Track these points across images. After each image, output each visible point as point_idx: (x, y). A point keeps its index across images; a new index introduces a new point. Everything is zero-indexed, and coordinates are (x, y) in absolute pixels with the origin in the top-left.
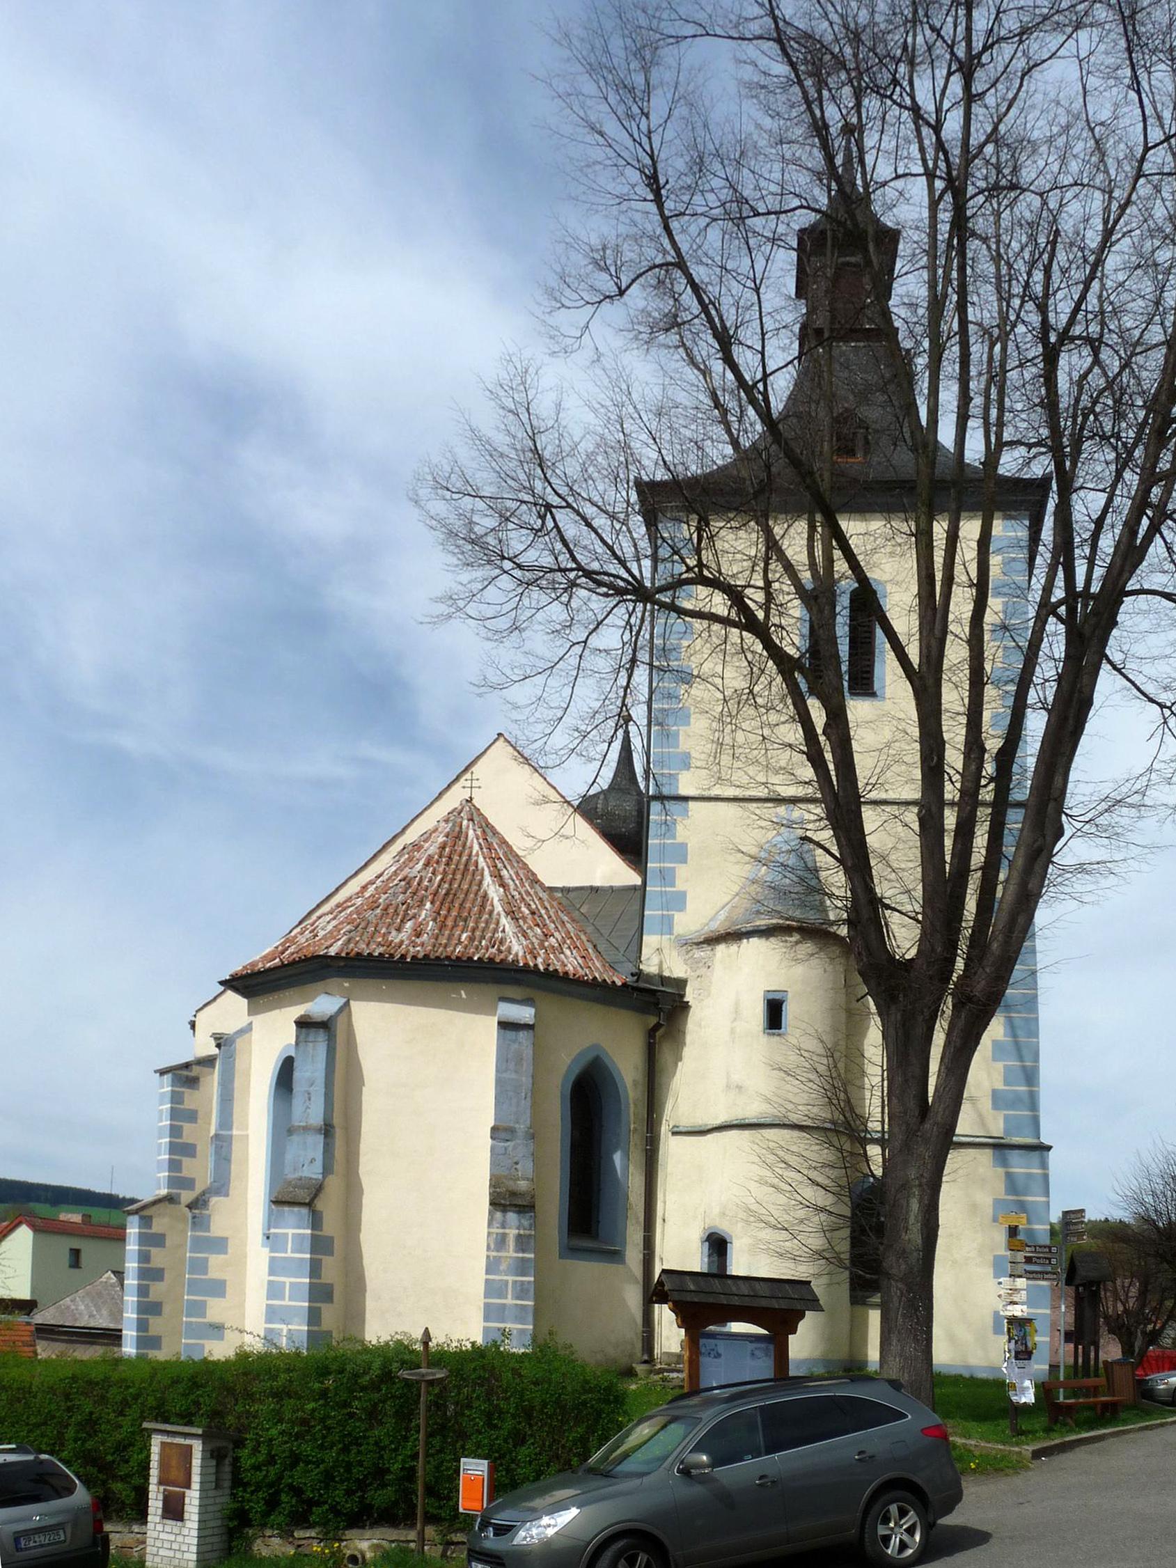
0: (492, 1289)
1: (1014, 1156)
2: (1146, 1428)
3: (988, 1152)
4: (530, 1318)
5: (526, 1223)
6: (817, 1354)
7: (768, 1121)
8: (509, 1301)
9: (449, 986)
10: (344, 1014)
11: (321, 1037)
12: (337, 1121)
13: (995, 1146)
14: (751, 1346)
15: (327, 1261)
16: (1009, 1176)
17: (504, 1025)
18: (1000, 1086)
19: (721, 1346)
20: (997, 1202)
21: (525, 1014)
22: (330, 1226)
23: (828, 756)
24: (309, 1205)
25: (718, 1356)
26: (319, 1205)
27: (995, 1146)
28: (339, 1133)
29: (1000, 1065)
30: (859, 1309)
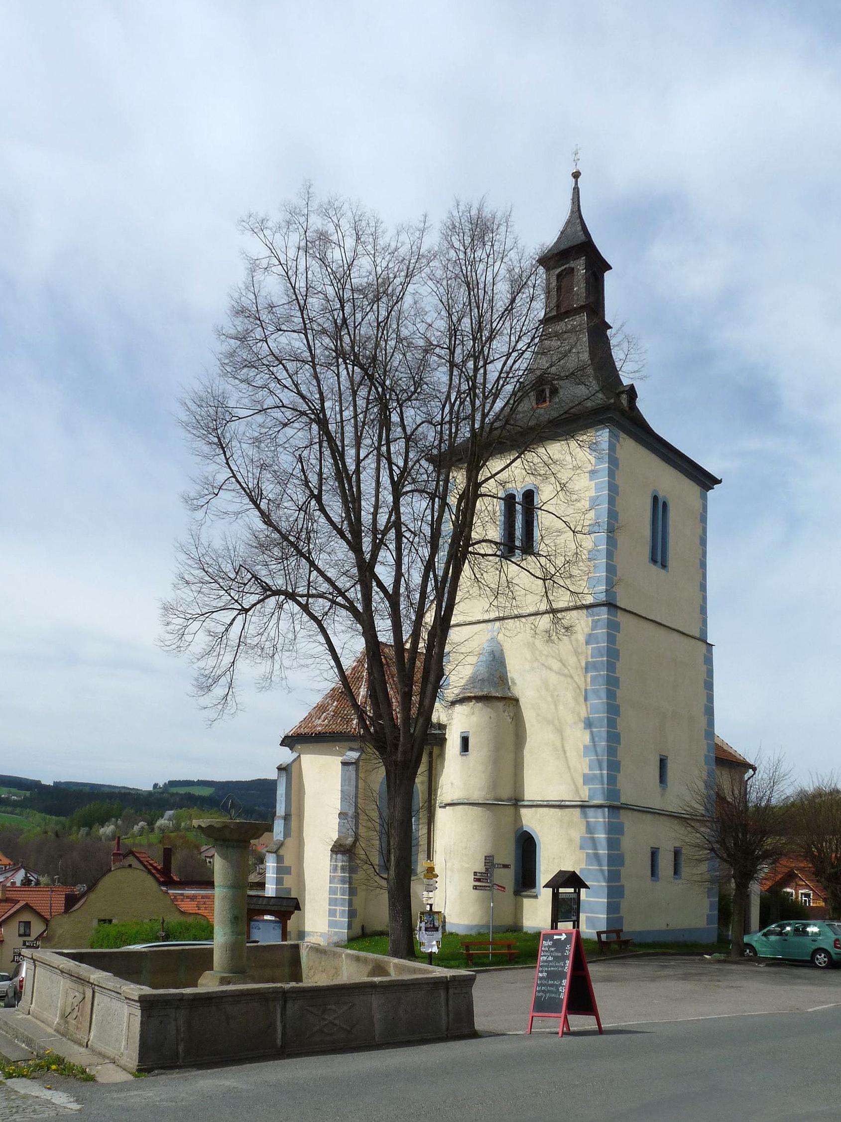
0: (332, 891)
1: (590, 812)
2: (528, 968)
3: (578, 810)
4: (347, 904)
5: (345, 859)
6: (483, 922)
7: (459, 801)
8: (339, 896)
9: (332, 744)
10: (298, 761)
11: (284, 774)
12: (294, 811)
13: (582, 807)
14: (273, 925)
15: (286, 877)
16: (587, 822)
17: (344, 764)
18: (587, 771)
19: (261, 925)
20: (581, 838)
21: (353, 755)
22: (287, 862)
23: (444, 605)
24: (275, 852)
25: (259, 929)
26: (281, 852)
27: (582, 807)
28: (294, 819)
29: (587, 759)
30: (519, 898)
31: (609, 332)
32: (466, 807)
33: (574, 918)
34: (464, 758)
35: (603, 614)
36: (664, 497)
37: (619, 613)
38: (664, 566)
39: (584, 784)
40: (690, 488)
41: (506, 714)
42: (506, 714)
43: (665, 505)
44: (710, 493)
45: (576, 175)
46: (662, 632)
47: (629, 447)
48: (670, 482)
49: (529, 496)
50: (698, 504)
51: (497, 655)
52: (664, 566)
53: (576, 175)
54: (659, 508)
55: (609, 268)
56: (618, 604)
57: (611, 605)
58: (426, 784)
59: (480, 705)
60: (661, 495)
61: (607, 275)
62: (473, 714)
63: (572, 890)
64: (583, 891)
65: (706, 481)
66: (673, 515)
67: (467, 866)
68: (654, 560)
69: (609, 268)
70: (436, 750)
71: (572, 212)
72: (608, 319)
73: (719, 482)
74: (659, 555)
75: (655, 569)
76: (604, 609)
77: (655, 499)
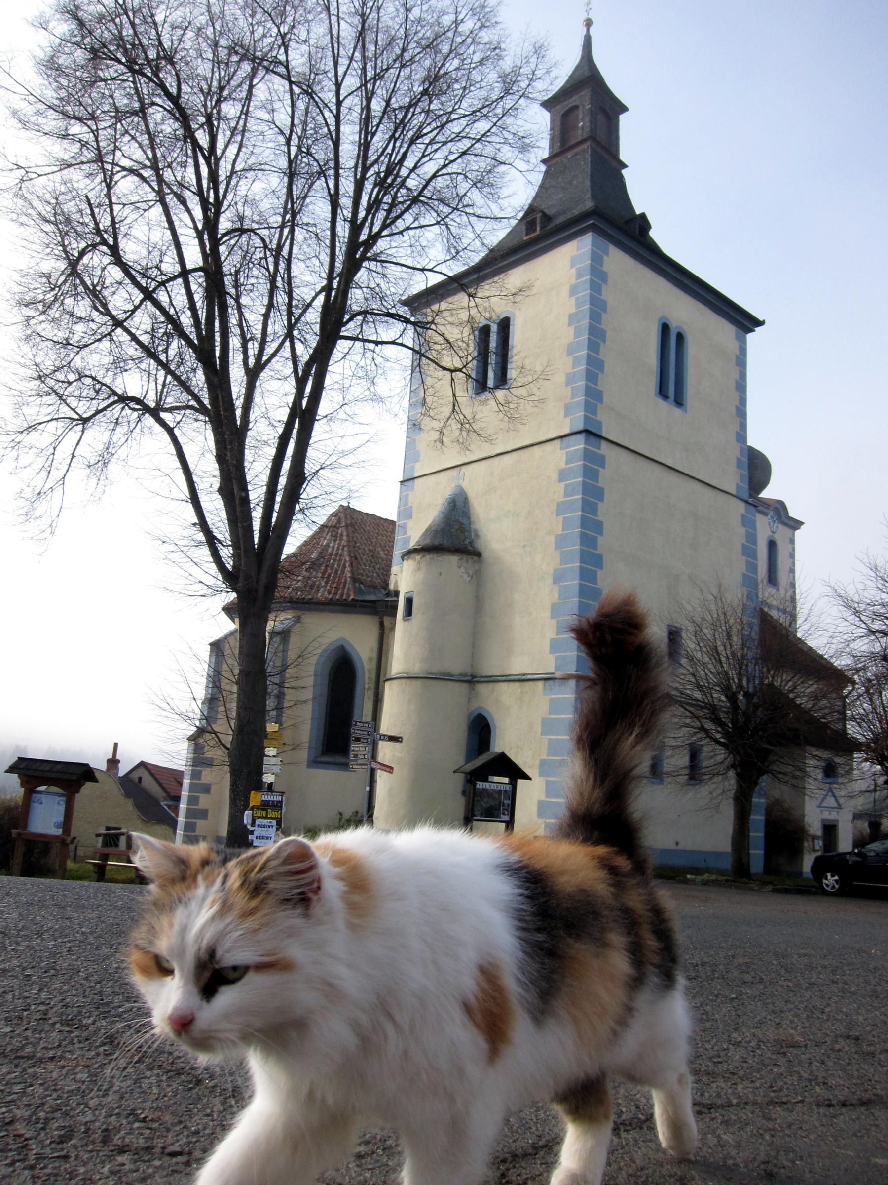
31: (624, 172)
32: (403, 681)
33: (507, 818)
34: (407, 622)
35: (579, 444)
36: (677, 327)
37: (604, 444)
38: (679, 402)
39: (551, 653)
40: (724, 330)
41: (462, 570)
42: (462, 570)
43: (680, 337)
44: (749, 336)
45: (589, 23)
46: (674, 478)
47: (618, 261)
48: (684, 311)
49: (505, 325)
50: (732, 345)
51: (459, 504)
52: (679, 402)
53: (589, 23)
54: (772, 545)
55: (624, 109)
56: (604, 435)
57: (591, 433)
58: (375, 662)
59: (428, 557)
60: (674, 325)
61: (622, 117)
62: (419, 569)
63: (506, 780)
64: (520, 782)
65: (746, 322)
66: (692, 350)
67: (400, 755)
68: (662, 392)
69: (624, 109)
70: (387, 621)
71: (583, 57)
72: (623, 157)
73: (760, 323)
74: (772, 578)
75: (665, 408)
76: (581, 438)
77: (665, 329)
